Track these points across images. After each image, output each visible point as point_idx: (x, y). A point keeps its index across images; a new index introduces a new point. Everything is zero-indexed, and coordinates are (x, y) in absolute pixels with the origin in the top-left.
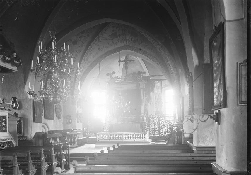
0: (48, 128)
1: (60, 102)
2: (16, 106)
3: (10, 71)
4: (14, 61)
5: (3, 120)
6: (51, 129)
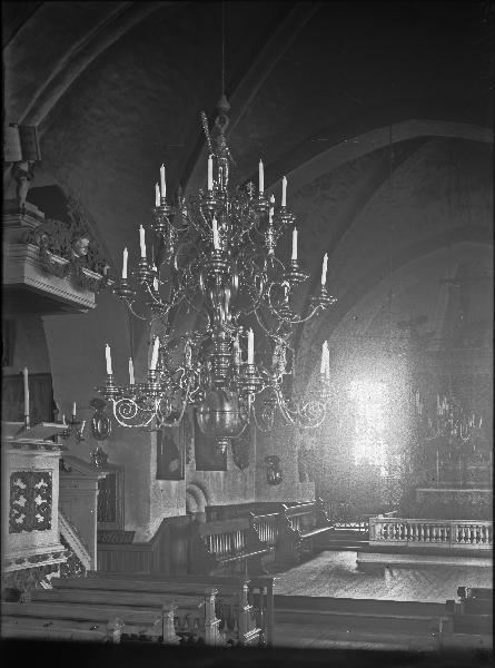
0: (207, 498)
3: (73, 307)
4: (81, 273)
5: (39, 486)
6: (214, 503)
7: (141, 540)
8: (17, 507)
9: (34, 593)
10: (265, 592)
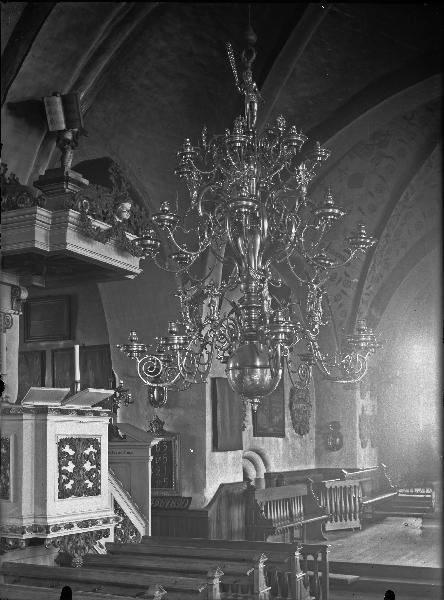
0: (266, 464)
1: (271, 389)
2: (161, 398)
5: (87, 452)
6: (274, 469)
7: (198, 507)
8: (65, 473)
9: (86, 557)
10: (320, 558)
